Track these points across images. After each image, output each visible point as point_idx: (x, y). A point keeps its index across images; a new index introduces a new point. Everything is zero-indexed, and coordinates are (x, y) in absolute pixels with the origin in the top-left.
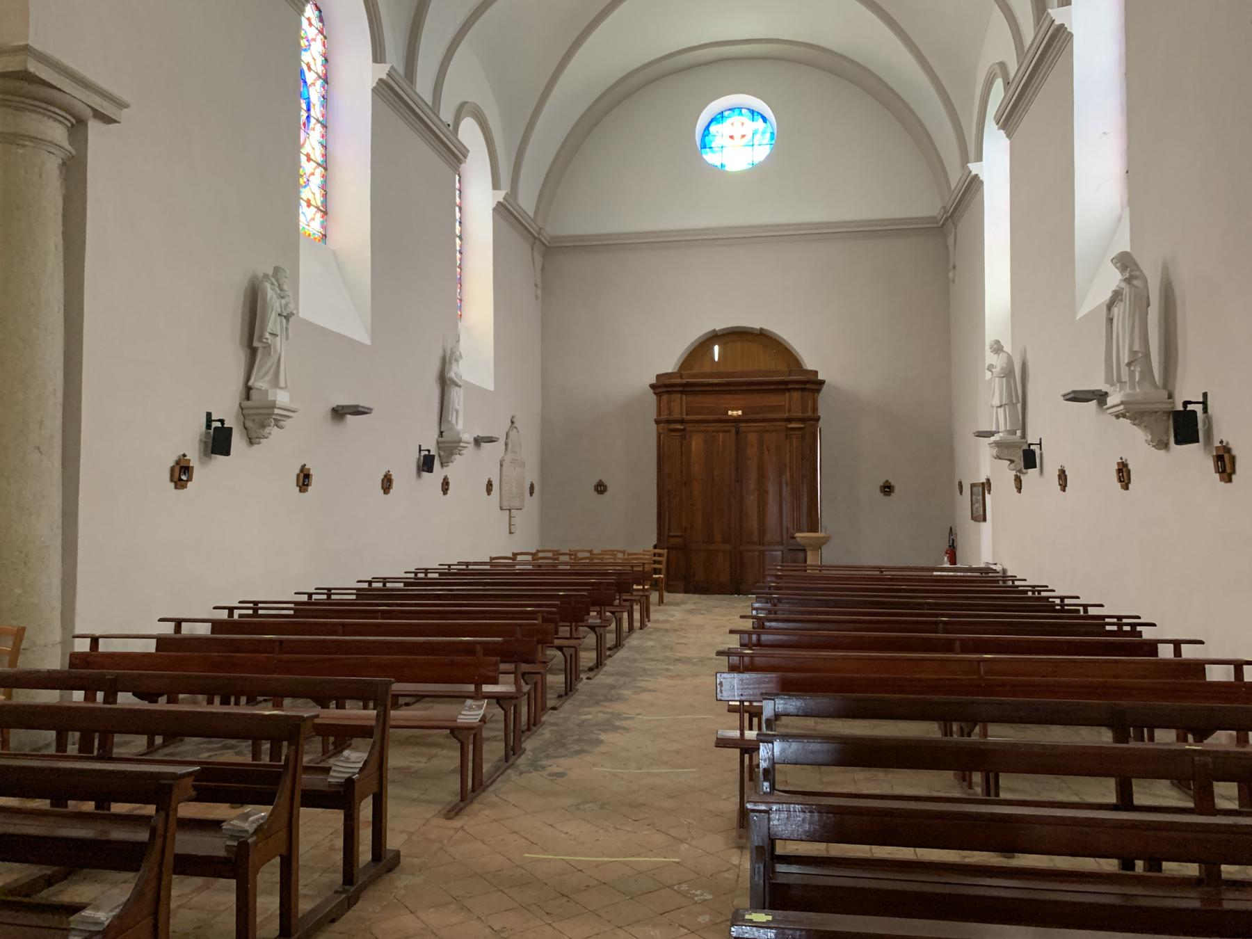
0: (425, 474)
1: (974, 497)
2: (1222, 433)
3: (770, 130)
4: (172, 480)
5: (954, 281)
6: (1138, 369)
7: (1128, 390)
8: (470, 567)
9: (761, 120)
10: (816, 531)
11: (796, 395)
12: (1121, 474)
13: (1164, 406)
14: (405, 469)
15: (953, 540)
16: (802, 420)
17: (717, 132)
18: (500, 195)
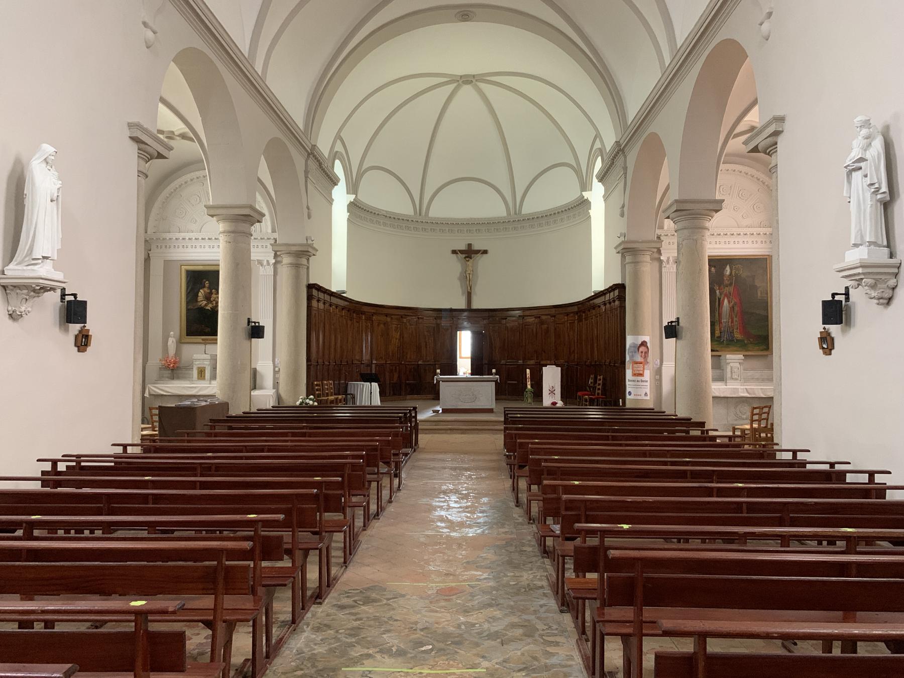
4: (76, 345)
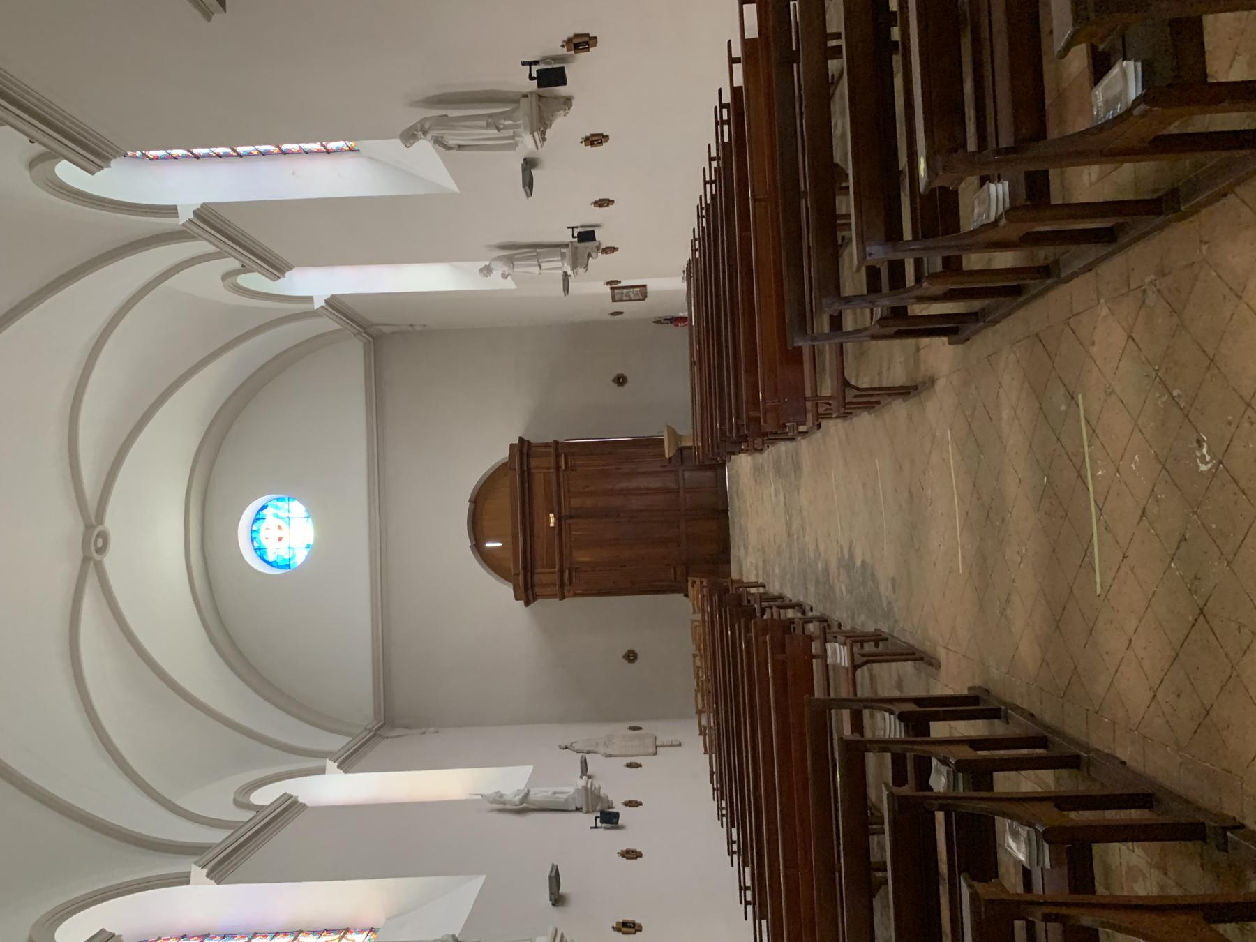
0: (620, 822)
1: (624, 299)
2: (555, 47)
3: (275, 502)
5: (424, 326)
6: (502, 121)
7: (521, 130)
8: (714, 770)
9: (265, 511)
10: (662, 440)
11: (533, 463)
12: (595, 142)
13: (534, 103)
14: (615, 840)
15: (666, 319)
16: (558, 456)
17: (274, 553)
18: (331, 765)
